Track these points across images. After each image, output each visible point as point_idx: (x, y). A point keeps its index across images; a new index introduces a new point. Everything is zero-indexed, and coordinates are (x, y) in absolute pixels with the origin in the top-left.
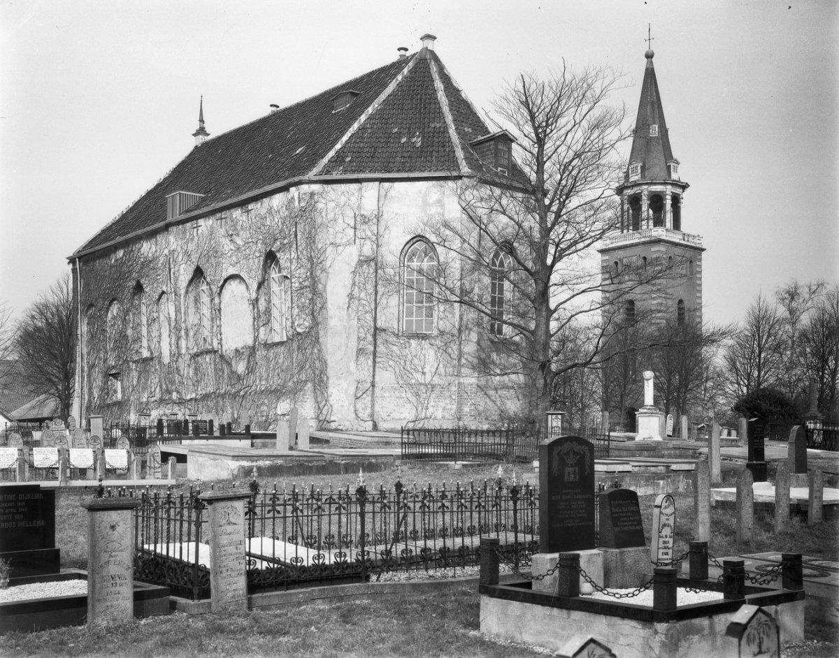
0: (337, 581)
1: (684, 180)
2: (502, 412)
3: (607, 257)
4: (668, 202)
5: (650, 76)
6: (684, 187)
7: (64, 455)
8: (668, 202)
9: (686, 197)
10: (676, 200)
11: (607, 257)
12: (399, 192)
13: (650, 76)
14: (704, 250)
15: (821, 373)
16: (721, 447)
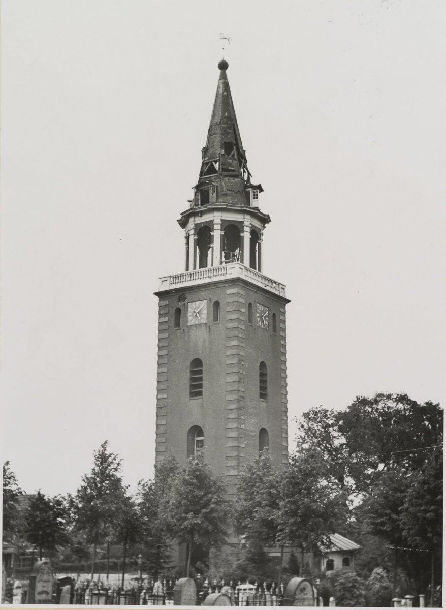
0: (237, 133)
1: (264, 210)
2: (165, 546)
3: (167, 303)
4: (247, 237)
5: (225, 101)
6: (265, 219)
7: (258, 317)
8: (247, 237)
9: (268, 234)
10: (256, 236)
11: (167, 303)
12: (276, 547)
13: (225, 101)
14: (289, 301)
15: (322, 448)
16: (168, 313)
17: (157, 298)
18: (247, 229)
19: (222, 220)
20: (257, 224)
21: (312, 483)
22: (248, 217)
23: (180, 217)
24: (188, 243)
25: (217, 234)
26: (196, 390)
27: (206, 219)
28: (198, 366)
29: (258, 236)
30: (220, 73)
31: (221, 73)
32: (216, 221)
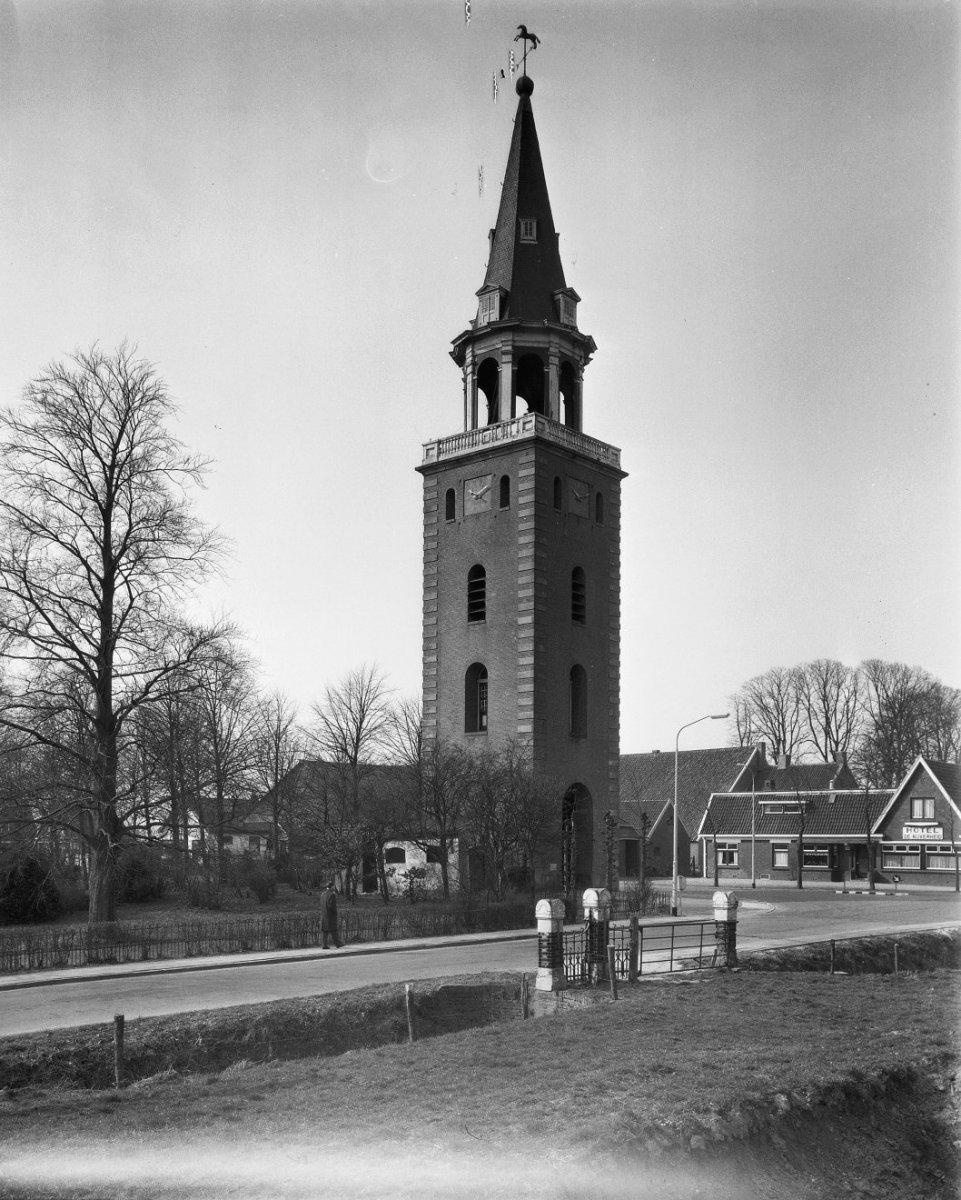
8: (553, 373)
17: (420, 477)
18: (555, 360)
19: (514, 347)
20: (567, 349)
21: (230, 678)
22: (555, 339)
23: (451, 348)
24: (466, 392)
25: (506, 373)
26: (476, 611)
27: (524, 341)
28: (480, 577)
29: (573, 370)
30: (518, 101)
31: (521, 101)
32: (552, 350)
